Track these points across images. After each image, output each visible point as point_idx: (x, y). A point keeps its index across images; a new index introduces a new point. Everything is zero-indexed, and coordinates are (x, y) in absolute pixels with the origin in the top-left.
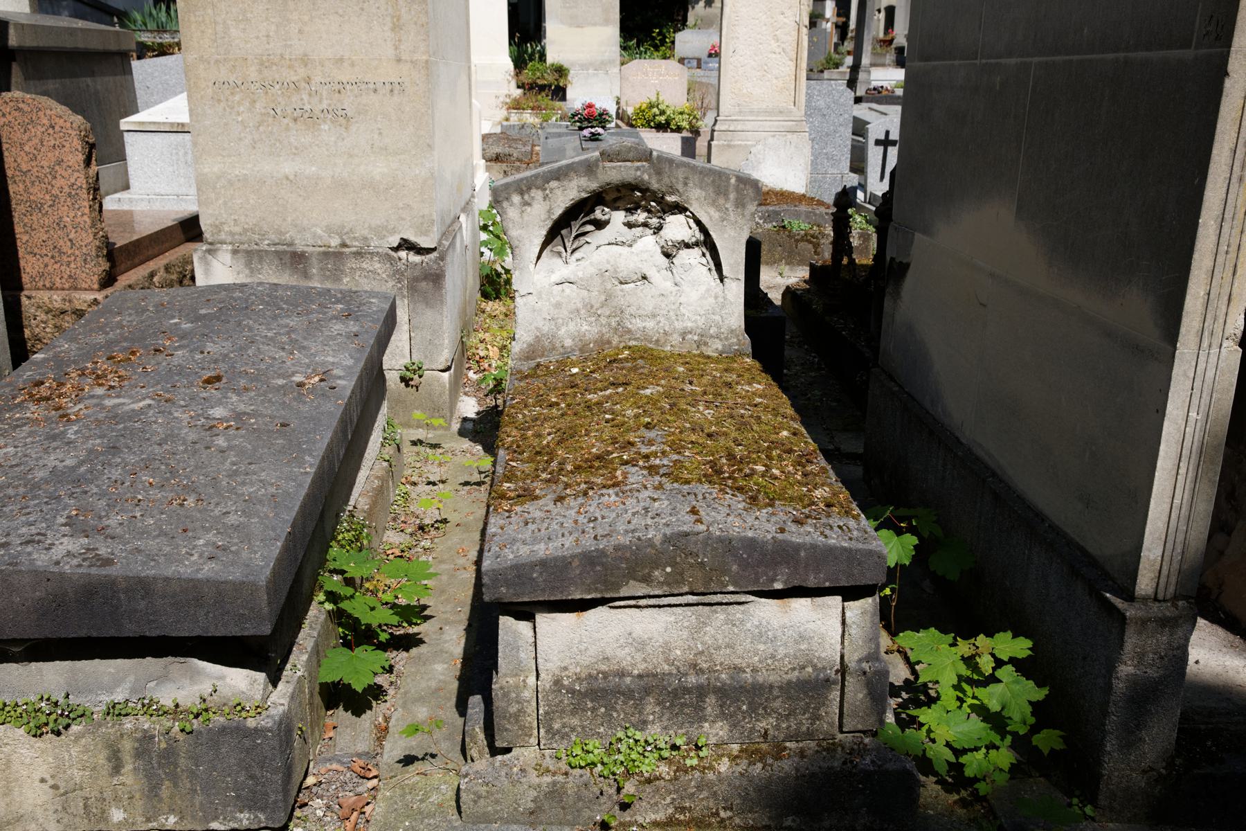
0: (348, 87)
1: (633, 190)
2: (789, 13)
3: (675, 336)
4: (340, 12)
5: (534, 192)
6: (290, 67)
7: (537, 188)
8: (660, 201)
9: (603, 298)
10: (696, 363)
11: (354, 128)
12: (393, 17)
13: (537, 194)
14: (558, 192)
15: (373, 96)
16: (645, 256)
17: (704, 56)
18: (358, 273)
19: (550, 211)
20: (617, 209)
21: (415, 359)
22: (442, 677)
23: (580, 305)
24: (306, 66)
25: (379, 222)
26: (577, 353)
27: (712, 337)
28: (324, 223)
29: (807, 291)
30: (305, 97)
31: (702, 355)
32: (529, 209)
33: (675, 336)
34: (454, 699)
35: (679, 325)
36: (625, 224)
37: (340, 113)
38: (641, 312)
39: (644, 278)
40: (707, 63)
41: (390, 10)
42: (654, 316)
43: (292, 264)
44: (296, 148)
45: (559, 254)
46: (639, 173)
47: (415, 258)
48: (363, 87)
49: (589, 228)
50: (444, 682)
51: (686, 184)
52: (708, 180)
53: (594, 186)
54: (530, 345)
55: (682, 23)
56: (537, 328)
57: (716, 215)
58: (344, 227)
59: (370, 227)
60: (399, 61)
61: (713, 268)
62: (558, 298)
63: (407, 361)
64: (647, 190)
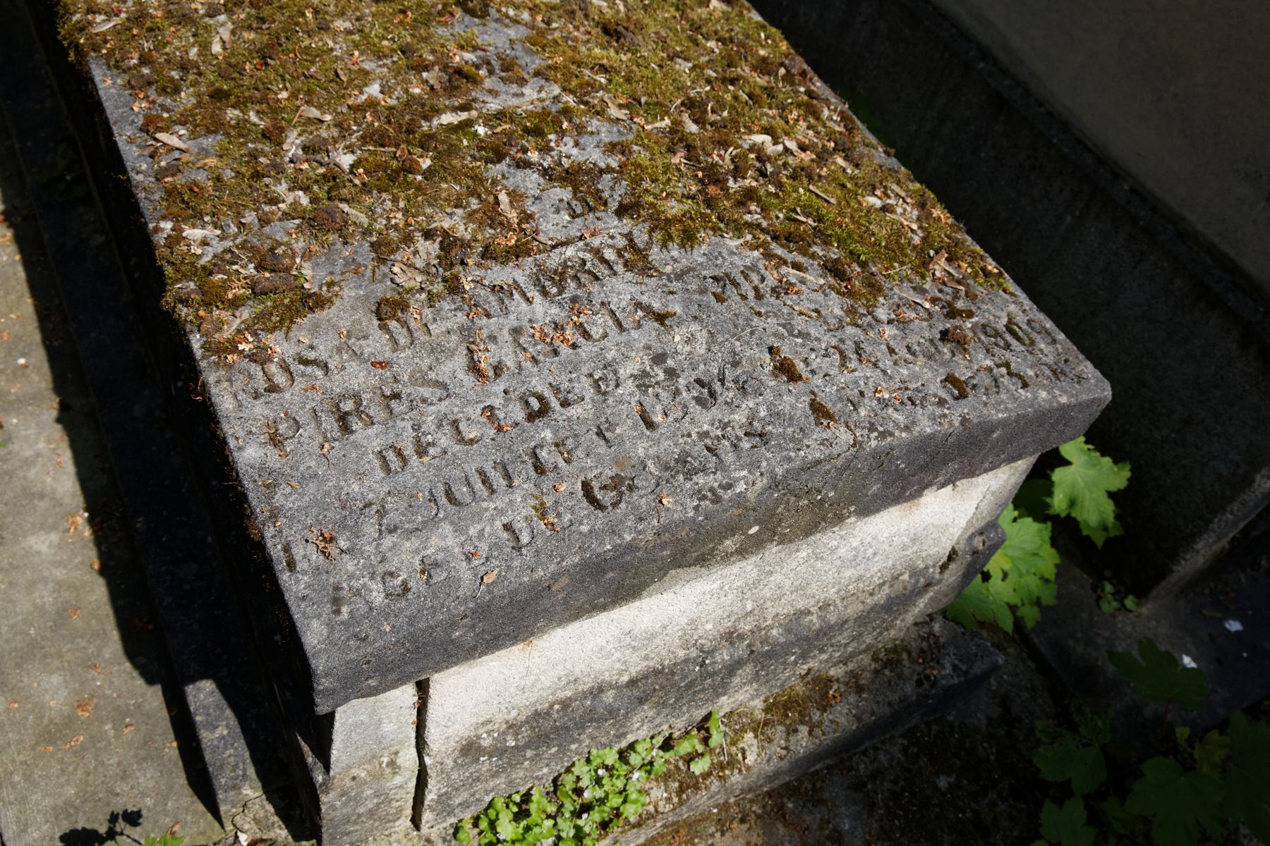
22: (59, 573)
34: (115, 635)
50: (71, 587)
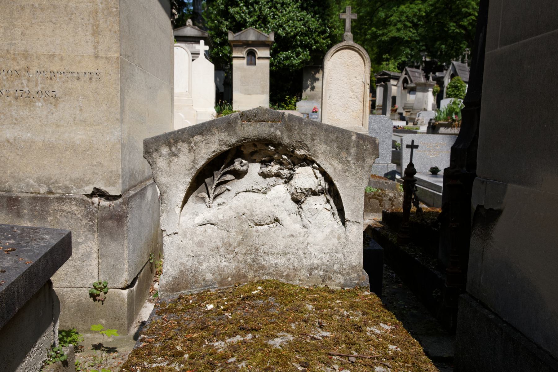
0: (58, 75)
1: (267, 145)
2: (359, 77)
3: (303, 271)
4: (54, 20)
5: (180, 145)
6: (14, 59)
7: (183, 141)
8: (291, 154)
9: (240, 237)
10: (322, 296)
11: (61, 105)
12: (93, 25)
13: (183, 147)
14: (202, 145)
15: (77, 84)
16: (277, 202)
17: (310, 112)
18: (60, 213)
19: (194, 162)
20: (254, 161)
21: (102, 281)
23: (219, 244)
24: (26, 59)
25: (77, 176)
26: (217, 286)
27: (335, 272)
28: (36, 176)
29: (383, 228)
30: (25, 82)
31: (326, 289)
32: (176, 160)
33: (303, 271)
35: (306, 262)
36: (260, 174)
37: (51, 94)
38: (273, 250)
39: (277, 220)
40: (311, 115)
41: (91, 20)
42: (285, 254)
43: (8, 206)
44: (16, 119)
45: (203, 199)
46: (272, 130)
47: (105, 203)
48: (69, 75)
49: (230, 177)
51: (313, 140)
52: (333, 137)
53: (233, 140)
54: (175, 278)
55: (300, 98)
56: (182, 264)
57: (339, 167)
58: (51, 179)
59: (71, 179)
60: (97, 57)
61: (336, 213)
62: (200, 238)
63: (95, 281)
64: (280, 144)
